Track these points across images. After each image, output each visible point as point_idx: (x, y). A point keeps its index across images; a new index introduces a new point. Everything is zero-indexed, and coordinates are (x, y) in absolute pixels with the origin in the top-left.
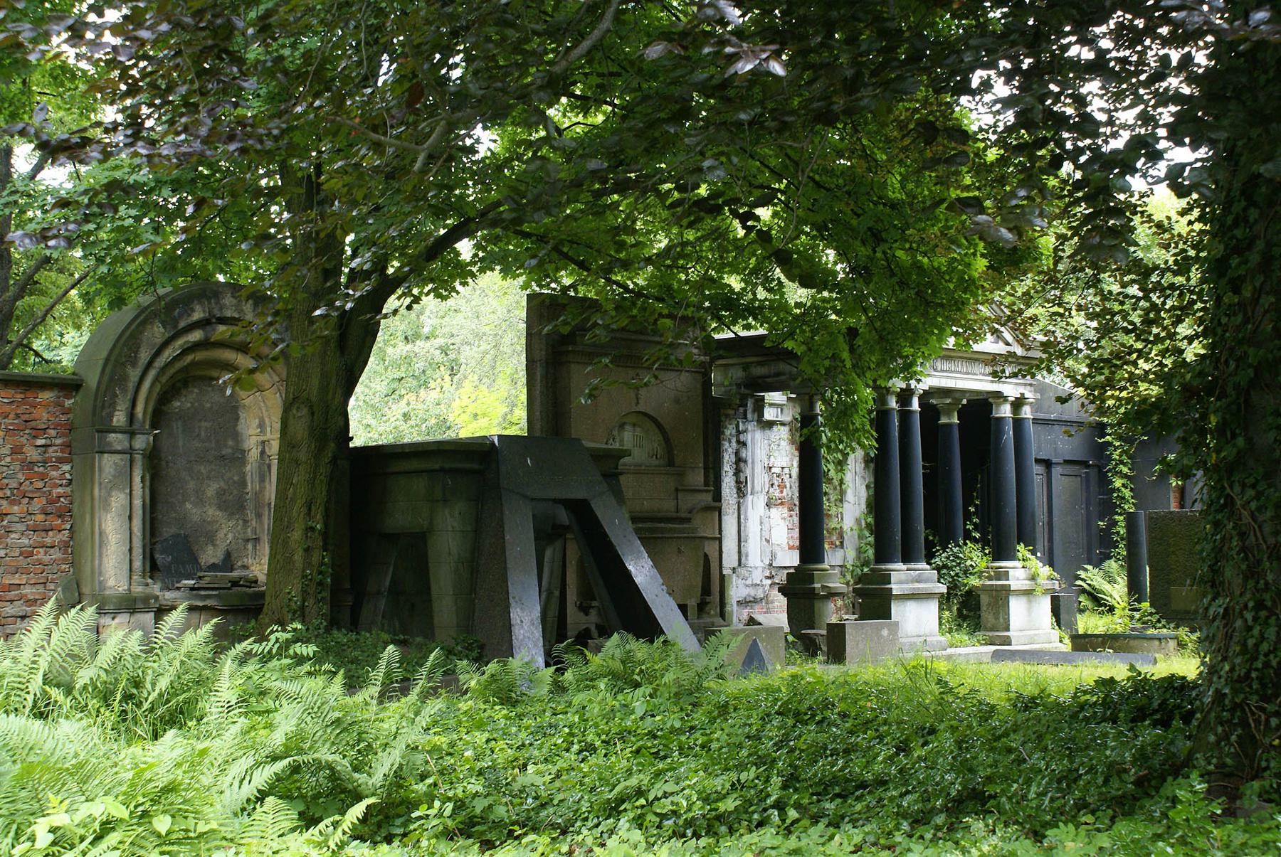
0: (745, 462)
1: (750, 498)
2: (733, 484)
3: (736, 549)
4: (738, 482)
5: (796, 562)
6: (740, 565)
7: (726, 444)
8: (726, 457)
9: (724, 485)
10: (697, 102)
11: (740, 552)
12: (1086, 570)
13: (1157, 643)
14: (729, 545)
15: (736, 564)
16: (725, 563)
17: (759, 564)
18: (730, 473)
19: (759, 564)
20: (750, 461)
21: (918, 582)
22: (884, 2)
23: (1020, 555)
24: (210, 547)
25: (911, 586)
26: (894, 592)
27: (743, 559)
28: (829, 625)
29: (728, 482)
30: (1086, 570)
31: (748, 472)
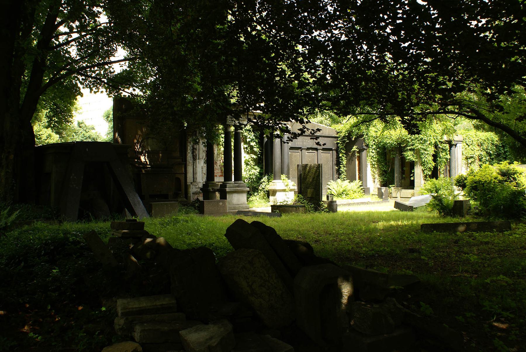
0: (196, 149)
1: (198, 161)
3: (193, 177)
4: (193, 156)
5: (223, 181)
6: (194, 181)
7: (189, 144)
8: (189, 148)
9: (188, 156)
10: (105, 40)
12: (331, 182)
13: (295, 208)
14: (190, 175)
15: (192, 181)
16: (188, 181)
17: (201, 181)
18: (191, 153)
19: (201, 181)
21: (238, 187)
22: (285, 2)
26: (227, 191)
29: (189, 155)
30: (331, 182)
31: (197, 152)
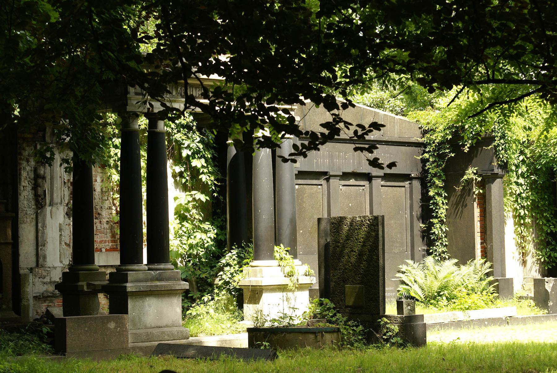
0: (44, 178)
1: (48, 209)
2: (31, 196)
3: (34, 252)
4: (36, 196)
6: (37, 265)
7: (24, 164)
8: (24, 174)
9: (21, 198)
11: (37, 255)
12: (407, 264)
15: (33, 265)
17: (58, 264)
18: (29, 188)
19: (58, 264)
20: (48, 178)
23: (277, 255)
24: (39, 188)
25: (149, 284)
26: (129, 289)
27: (41, 260)
28: (110, 313)
30: (407, 264)
31: (47, 186)
